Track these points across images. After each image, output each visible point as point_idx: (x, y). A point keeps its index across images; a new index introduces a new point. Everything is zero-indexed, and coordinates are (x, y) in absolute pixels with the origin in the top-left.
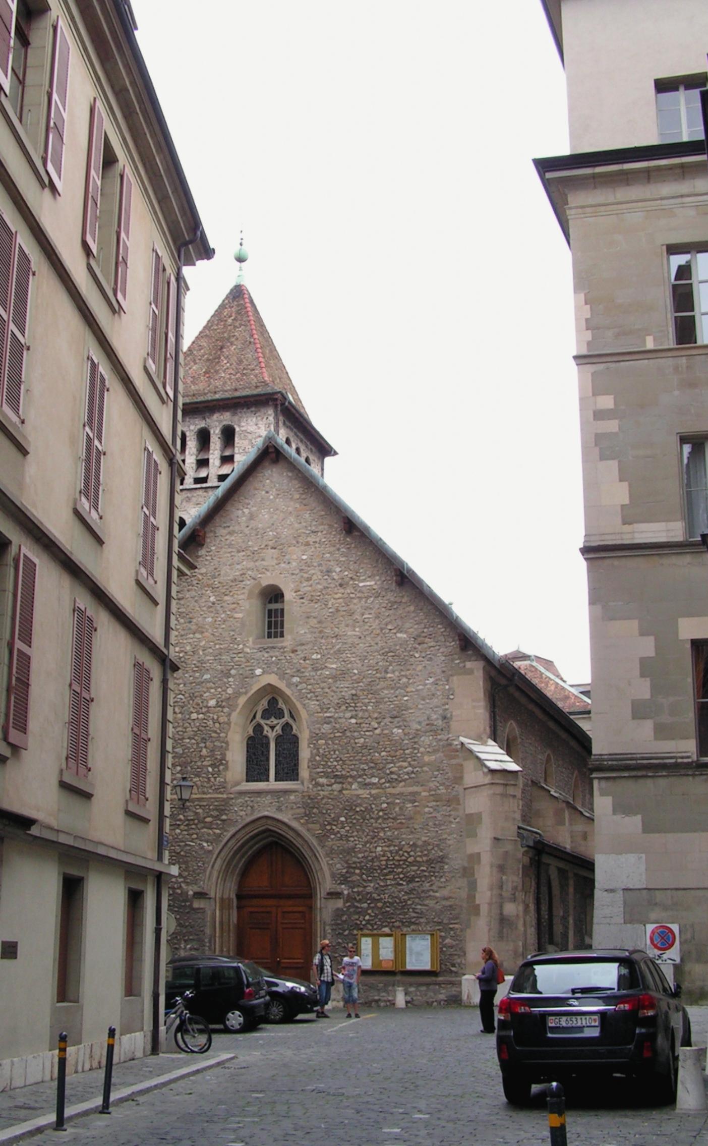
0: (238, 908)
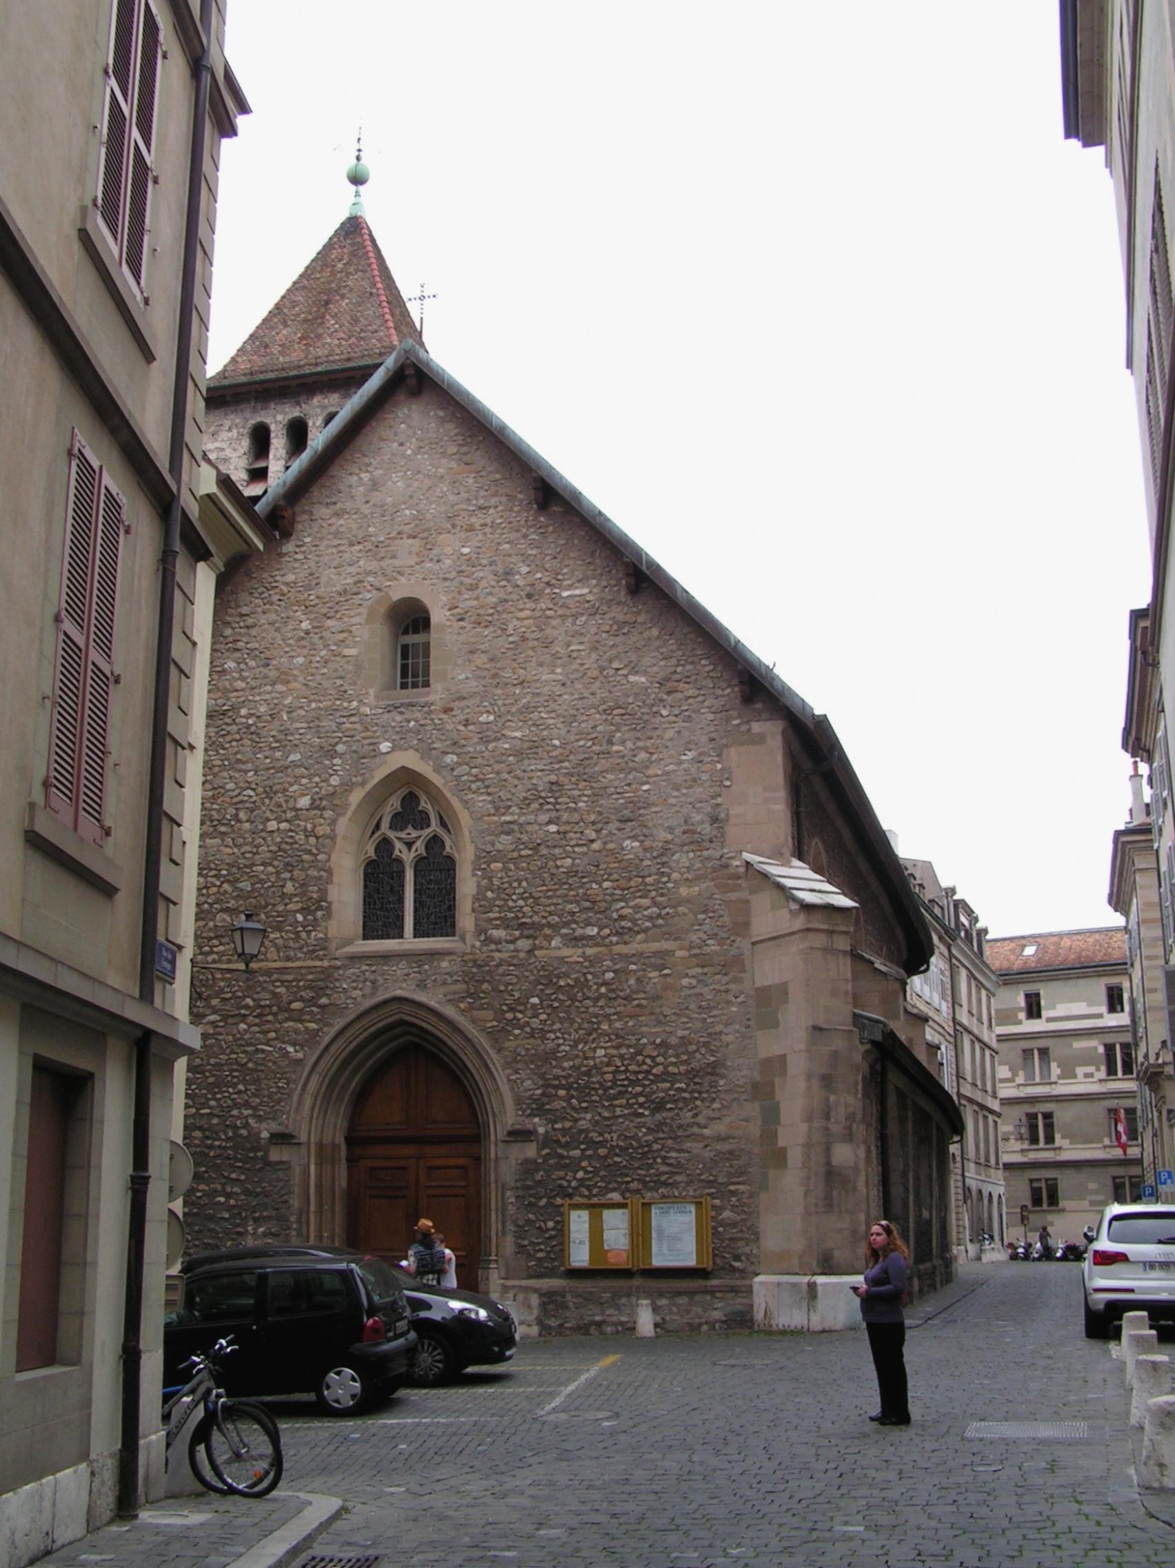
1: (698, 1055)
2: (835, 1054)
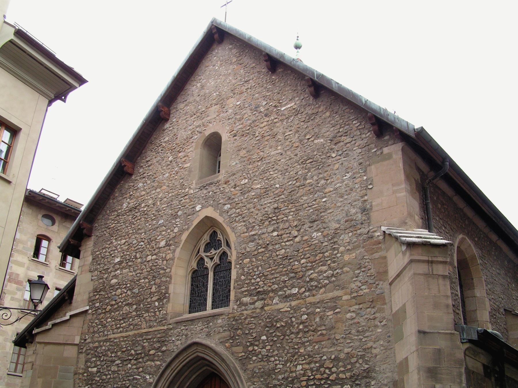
1: (358, 365)
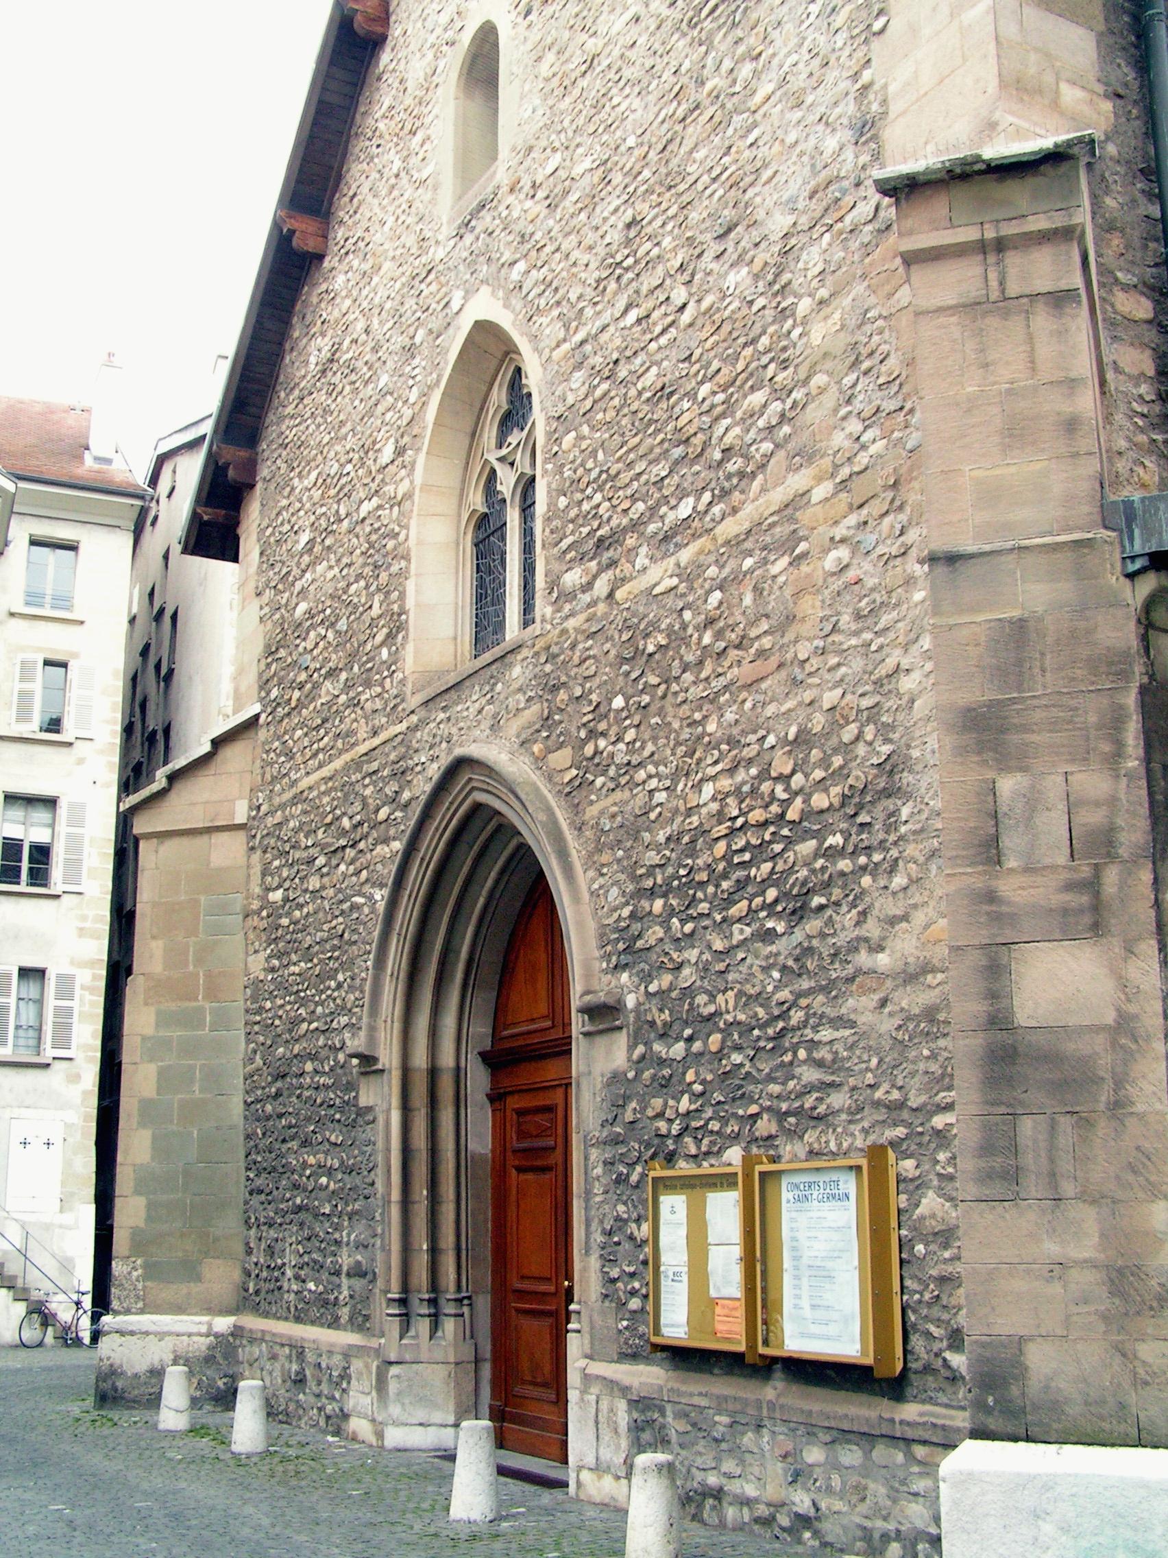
0: (496, 1098)
1: (861, 749)
2: (1018, 632)
